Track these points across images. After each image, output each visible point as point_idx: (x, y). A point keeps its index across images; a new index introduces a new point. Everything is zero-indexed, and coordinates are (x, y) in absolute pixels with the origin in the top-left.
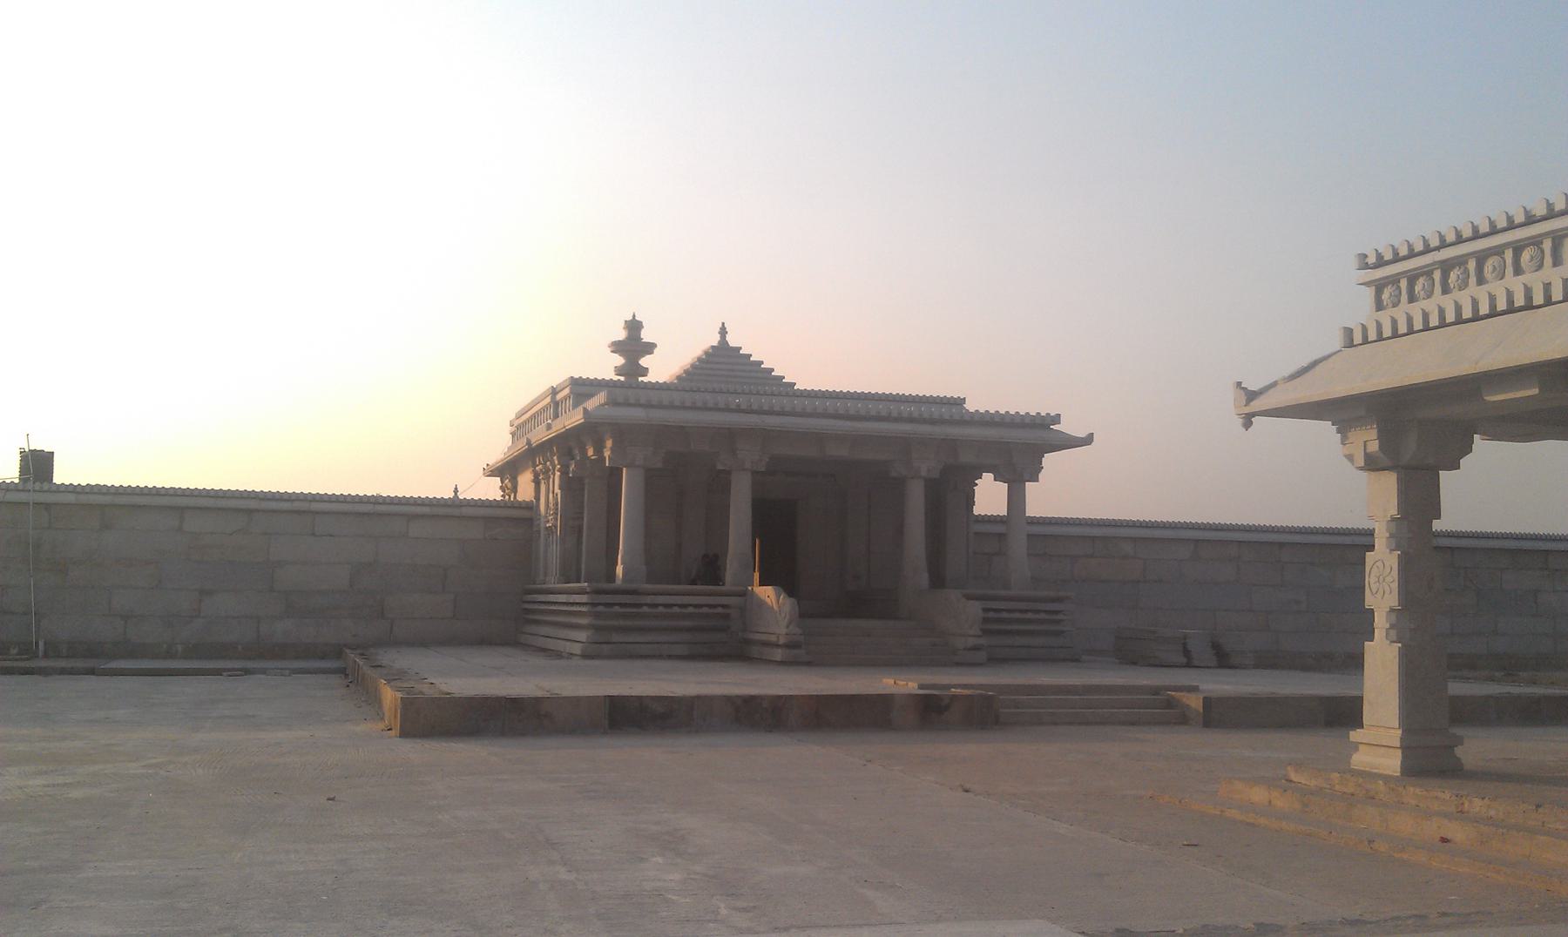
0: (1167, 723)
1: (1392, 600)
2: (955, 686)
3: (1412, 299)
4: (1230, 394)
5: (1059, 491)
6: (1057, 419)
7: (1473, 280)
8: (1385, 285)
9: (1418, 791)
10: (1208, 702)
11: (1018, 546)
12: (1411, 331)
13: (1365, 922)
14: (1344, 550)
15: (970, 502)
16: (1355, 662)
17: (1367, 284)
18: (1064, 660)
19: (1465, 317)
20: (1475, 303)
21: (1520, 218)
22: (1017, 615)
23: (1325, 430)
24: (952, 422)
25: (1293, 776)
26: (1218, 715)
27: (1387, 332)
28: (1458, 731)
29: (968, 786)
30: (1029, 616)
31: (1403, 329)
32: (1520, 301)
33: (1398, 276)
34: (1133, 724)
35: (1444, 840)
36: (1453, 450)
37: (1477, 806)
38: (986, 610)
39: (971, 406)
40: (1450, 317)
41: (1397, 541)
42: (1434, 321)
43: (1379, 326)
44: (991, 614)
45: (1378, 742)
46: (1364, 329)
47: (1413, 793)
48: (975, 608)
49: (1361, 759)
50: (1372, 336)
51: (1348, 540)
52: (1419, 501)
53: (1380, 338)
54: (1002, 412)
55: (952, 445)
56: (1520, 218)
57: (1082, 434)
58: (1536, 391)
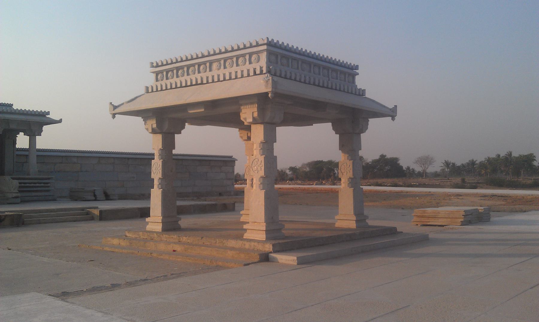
0: (87, 220)
1: (160, 175)
2: (7, 212)
3: (167, 79)
4: (108, 107)
5: (49, 140)
6: (48, 113)
7: (186, 74)
8: (159, 73)
9: (167, 236)
10: (101, 212)
11: (33, 160)
12: (166, 89)
13: (147, 280)
14: (143, 160)
15: (15, 143)
16: (147, 197)
17: (153, 72)
18: (50, 200)
19: (227, 79)
20: (186, 81)
21: (200, 55)
22: (32, 185)
23: (139, 120)
24: (7, 113)
25: (127, 235)
26: (104, 216)
27: (159, 89)
28: (180, 217)
29: (10, 248)
30: (37, 185)
31: (164, 88)
32: (199, 82)
33: (164, 71)
34: (75, 221)
35: (174, 251)
36: (179, 129)
37: (184, 239)
38: (20, 183)
39: (15, 107)
40: (179, 85)
41: (161, 156)
42: (174, 86)
43: (157, 87)
44: (23, 185)
45: (155, 222)
46: (152, 87)
47: (165, 237)
48: (16, 183)
49: (149, 227)
50: (155, 90)
51: (63, 154)
52: (168, 144)
53: (157, 91)
54: (27, 110)
55: (8, 121)
56: (254, 44)
57: (58, 119)
58: (203, 110)
